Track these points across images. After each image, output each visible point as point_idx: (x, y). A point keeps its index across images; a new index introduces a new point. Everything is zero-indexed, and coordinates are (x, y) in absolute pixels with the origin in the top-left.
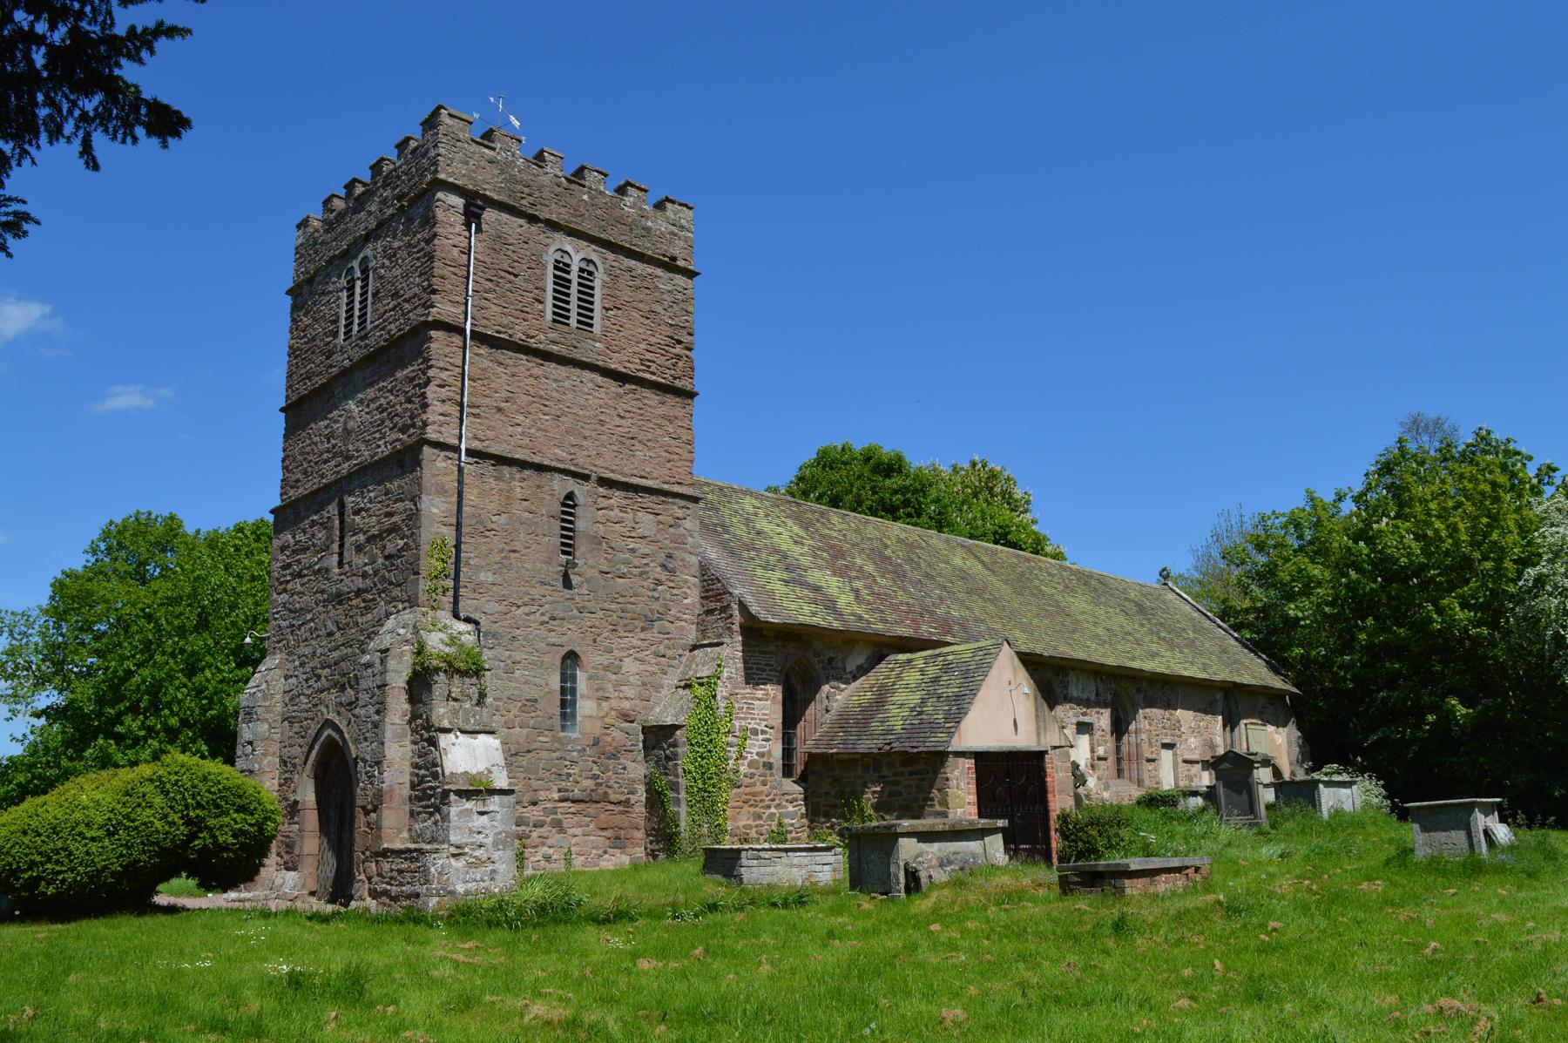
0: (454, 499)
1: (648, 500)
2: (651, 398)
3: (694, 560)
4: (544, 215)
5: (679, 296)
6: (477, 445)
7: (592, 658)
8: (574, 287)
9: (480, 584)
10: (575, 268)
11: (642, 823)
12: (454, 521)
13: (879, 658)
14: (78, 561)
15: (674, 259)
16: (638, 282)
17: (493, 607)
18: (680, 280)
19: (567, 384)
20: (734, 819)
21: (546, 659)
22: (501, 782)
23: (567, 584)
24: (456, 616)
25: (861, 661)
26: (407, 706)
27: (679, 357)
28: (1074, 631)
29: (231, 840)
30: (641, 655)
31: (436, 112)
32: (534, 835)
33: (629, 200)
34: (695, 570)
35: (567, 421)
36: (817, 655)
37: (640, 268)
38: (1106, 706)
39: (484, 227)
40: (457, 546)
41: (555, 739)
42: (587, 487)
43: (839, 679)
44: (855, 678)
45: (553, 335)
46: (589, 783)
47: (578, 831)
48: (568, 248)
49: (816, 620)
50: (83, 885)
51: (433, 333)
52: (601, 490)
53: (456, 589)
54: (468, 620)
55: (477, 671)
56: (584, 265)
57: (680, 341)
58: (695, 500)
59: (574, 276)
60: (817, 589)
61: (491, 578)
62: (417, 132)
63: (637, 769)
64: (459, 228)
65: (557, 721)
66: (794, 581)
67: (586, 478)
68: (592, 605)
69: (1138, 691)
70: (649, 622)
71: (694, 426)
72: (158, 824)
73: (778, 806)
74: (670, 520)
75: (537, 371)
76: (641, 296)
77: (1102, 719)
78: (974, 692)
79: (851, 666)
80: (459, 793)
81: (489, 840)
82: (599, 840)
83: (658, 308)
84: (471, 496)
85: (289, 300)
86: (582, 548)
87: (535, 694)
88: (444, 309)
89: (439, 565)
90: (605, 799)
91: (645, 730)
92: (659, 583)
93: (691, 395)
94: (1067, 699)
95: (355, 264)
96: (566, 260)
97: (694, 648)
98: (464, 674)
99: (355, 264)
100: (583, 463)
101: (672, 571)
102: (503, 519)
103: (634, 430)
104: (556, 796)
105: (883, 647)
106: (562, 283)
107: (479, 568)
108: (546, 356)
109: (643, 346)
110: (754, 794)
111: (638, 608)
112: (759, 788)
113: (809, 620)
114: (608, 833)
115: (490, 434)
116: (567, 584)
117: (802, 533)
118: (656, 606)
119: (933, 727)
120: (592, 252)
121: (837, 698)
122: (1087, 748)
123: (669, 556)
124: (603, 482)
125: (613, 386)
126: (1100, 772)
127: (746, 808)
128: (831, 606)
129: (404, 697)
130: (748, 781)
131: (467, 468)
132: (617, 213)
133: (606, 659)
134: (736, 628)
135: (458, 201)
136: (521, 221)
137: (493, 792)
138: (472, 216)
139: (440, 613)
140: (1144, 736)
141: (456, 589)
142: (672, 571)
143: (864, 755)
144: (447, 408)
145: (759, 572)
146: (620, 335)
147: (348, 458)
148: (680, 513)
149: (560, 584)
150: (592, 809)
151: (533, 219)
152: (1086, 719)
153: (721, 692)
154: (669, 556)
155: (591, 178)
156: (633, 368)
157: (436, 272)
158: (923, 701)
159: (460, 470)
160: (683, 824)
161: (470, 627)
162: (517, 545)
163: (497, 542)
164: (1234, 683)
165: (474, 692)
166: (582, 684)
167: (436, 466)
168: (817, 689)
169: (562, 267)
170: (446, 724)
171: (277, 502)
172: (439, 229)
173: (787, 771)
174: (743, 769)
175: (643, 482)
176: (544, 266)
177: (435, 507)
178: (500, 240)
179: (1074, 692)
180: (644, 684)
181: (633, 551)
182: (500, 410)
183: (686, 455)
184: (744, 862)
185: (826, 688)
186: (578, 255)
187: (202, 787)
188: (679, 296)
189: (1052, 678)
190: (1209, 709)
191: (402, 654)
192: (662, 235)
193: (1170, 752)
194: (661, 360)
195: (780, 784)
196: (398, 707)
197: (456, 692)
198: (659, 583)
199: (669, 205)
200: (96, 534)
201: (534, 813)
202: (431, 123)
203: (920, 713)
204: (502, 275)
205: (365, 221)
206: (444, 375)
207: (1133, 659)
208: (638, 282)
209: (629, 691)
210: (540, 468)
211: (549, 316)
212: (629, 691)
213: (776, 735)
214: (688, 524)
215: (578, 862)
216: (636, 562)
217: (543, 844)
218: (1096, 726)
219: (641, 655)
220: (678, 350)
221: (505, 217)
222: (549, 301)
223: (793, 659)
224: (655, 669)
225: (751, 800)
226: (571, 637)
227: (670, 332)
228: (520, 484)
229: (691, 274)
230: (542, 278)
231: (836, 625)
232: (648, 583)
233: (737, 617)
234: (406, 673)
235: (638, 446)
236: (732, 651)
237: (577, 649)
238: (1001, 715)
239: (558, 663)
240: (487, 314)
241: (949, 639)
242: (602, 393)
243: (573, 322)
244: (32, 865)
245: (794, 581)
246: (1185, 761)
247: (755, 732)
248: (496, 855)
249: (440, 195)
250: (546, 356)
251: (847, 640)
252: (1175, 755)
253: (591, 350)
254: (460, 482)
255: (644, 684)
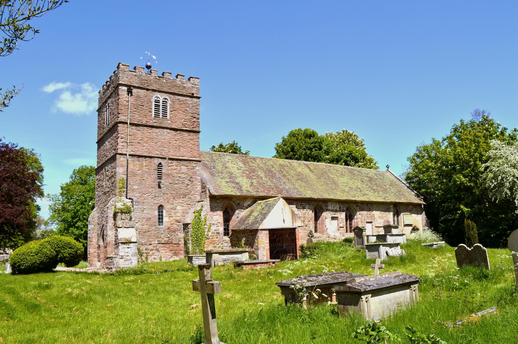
0: (126, 167)
1: (184, 163)
2: (186, 134)
3: (199, 178)
5: (195, 105)
6: (132, 153)
8: (161, 108)
9: (134, 189)
10: (161, 102)
11: (183, 249)
13: (255, 202)
14: (68, 180)
15: (193, 94)
16: (181, 102)
17: (138, 195)
18: (195, 100)
19: (159, 134)
20: (207, 248)
21: (154, 207)
23: (159, 187)
24: (127, 198)
25: (249, 203)
26: (113, 221)
27: (195, 122)
29: (68, 255)
30: (183, 205)
31: (119, 65)
32: (151, 253)
33: (178, 79)
34: (200, 180)
35: (159, 144)
36: (234, 202)
38: (343, 211)
39: (133, 94)
40: (127, 180)
41: (156, 228)
42: (165, 161)
43: (242, 208)
44: (247, 208)
46: (167, 239)
47: (164, 251)
48: (159, 96)
50: (30, 266)
51: (119, 125)
52: (170, 161)
53: (127, 191)
54: (130, 199)
55: (129, 212)
56: (164, 100)
57: (195, 117)
58: (200, 161)
59: (161, 104)
61: (137, 187)
62: (116, 69)
63: (181, 235)
64: (126, 95)
65: (157, 223)
67: (165, 158)
68: (167, 192)
69: (357, 206)
70: (185, 196)
71: (200, 141)
72: (48, 252)
73: (222, 244)
74: (192, 168)
75: (150, 131)
76: (182, 106)
77: (342, 216)
79: (246, 204)
80: (122, 243)
81: (130, 255)
82: (170, 254)
83: (188, 109)
84: (131, 167)
85: (97, 113)
86: (164, 177)
87: (150, 216)
88: (122, 118)
89: (122, 185)
90: (171, 243)
91: (184, 225)
92: (188, 185)
93: (199, 132)
94: (327, 210)
95: (107, 104)
96: (159, 99)
97: (199, 202)
98: (126, 213)
99: (107, 104)
100: (164, 155)
101: (192, 181)
102: (140, 172)
103: (180, 144)
104: (157, 243)
105: (255, 199)
106: (157, 106)
107: (134, 185)
108: (153, 127)
109: (183, 120)
110: (214, 241)
111: (181, 192)
112: (215, 239)
114: (173, 252)
115: (136, 149)
116: (159, 187)
118: (187, 191)
120: (166, 96)
121: (240, 214)
123: (191, 177)
124: (170, 159)
125: (173, 132)
126: (340, 231)
127: (211, 245)
129: (112, 219)
130: (211, 237)
131: (129, 159)
132: (175, 84)
133: (171, 206)
134: (208, 196)
135: (125, 88)
136: (145, 91)
137: (131, 243)
138: (130, 92)
139: (122, 197)
140: (359, 220)
141: (127, 191)
142: (192, 181)
143: (242, 230)
144: (123, 144)
145: (219, 180)
146: (176, 117)
147: (107, 157)
148: (195, 165)
149: (157, 188)
150: (168, 246)
151: (148, 90)
152: (335, 216)
153: (203, 214)
154: (191, 177)
155: (166, 75)
156: (180, 127)
157: (119, 108)
159: (127, 160)
160: (190, 249)
161: (130, 200)
162: (144, 178)
163: (138, 178)
165: (129, 217)
167: (120, 160)
168: (235, 212)
169: (157, 101)
170: (120, 226)
172: (120, 97)
173: (226, 233)
174: (210, 234)
175: (184, 158)
176: (152, 102)
177: (120, 171)
178: (138, 97)
179: (330, 208)
181: (180, 177)
182: (139, 143)
183: (197, 149)
184: (194, 259)
185: (237, 211)
186: (161, 97)
187: (60, 243)
188: (195, 105)
190: (388, 210)
191: (112, 209)
192: (189, 88)
193: (370, 224)
195: (222, 238)
196: (111, 221)
197: (123, 218)
198: (188, 185)
199: (191, 79)
200: (71, 173)
201: (151, 247)
202: (118, 67)
204: (139, 106)
205: (108, 93)
206: (122, 135)
208: (181, 102)
209: (178, 214)
210: (151, 157)
211: (153, 116)
212: (178, 214)
214: (197, 168)
215: (163, 260)
216: (181, 180)
218: (339, 217)
219: (183, 205)
220: (194, 120)
221: (139, 90)
222: (153, 111)
223: (226, 205)
224: (187, 208)
225: (213, 243)
226: (161, 201)
227: (192, 115)
229: (199, 98)
230: (151, 105)
232: (185, 185)
233: (208, 194)
234: (113, 213)
236: (207, 202)
237: (163, 204)
239: (157, 208)
240: (135, 117)
242: (170, 135)
243: (161, 116)
244: (19, 262)
247: (214, 224)
249: (120, 87)
250: (153, 127)
251: (245, 198)
252: (372, 225)
253: (167, 123)
254: (128, 163)
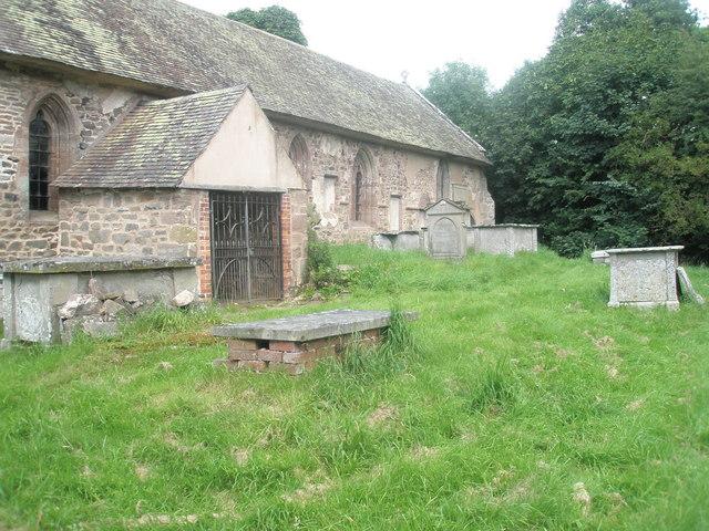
28: (327, 103)
49: (68, 59)
60: (79, 35)
66: (54, 24)
78: (212, 133)
119: (169, 165)
122: (333, 195)
128: (88, 49)
158: (166, 141)
164: (448, 153)
189: (296, 131)
203: (161, 152)
207: (373, 129)
231: (87, 65)
238: (244, 155)
245: (54, 24)
246: (408, 209)
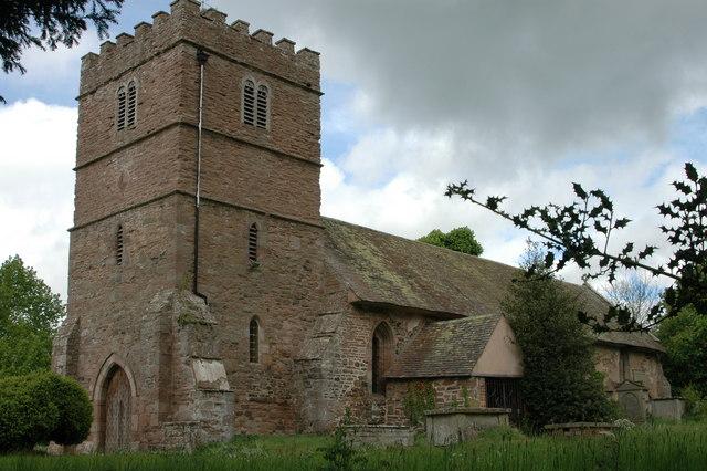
4: (239, 60)
7: (267, 320)
8: (256, 102)
10: (256, 91)
12: (192, 239)
15: (309, 85)
17: (213, 289)
22: (225, 386)
37: (288, 88)
45: (245, 131)
46: (265, 392)
47: (260, 419)
48: (253, 79)
54: (201, 296)
78: (485, 343)
84: (202, 226)
86: (260, 257)
92: (302, 276)
106: (249, 100)
113: (388, 300)
117: (376, 249)
123: (308, 262)
148: (313, 236)
156: (286, 150)
166: (261, 334)
171: (72, 225)
180: (295, 335)
194: (303, 146)
198: (302, 276)
209: (287, 340)
211: (243, 120)
213: (369, 367)
217: (241, 426)
228: (226, 218)
230: (238, 97)
235: (290, 197)
241: (465, 314)
248: (225, 428)
250: (241, 142)
253: (265, 139)
254: (197, 216)
255: (295, 335)
